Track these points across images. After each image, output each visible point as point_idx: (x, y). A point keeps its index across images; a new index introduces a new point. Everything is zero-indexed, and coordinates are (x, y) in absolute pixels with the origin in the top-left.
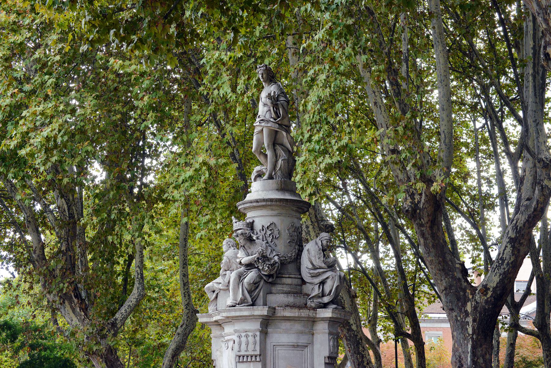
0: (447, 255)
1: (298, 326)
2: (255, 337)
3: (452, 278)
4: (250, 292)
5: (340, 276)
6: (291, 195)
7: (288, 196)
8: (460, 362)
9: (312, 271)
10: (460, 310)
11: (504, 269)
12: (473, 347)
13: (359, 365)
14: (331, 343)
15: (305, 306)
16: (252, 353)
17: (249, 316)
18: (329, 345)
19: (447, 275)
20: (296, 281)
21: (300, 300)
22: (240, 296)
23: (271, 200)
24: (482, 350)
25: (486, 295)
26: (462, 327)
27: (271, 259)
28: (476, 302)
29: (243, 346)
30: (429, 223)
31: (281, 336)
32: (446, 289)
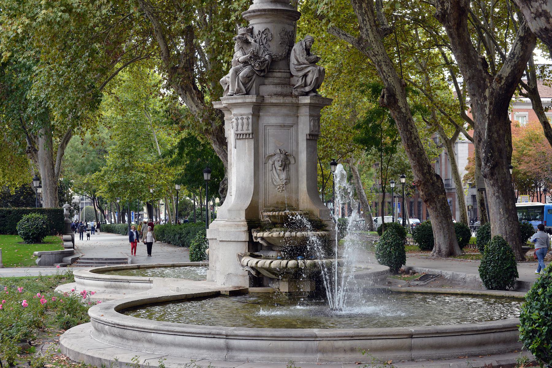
0: (471, 51)
1: (284, 111)
2: (248, 119)
3: (475, 69)
4: (244, 84)
5: (319, 70)
6: (282, 5)
7: (279, 7)
8: (479, 136)
9: (297, 67)
10: (481, 96)
11: (515, 62)
12: (489, 125)
13: (408, 140)
14: (312, 123)
15: (291, 95)
16: (246, 132)
17: (243, 103)
18: (310, 125)
19: (470, 67)
20: (284, 75)
21: (286, 90)
22: (236, 87)
23: (264, 10)
24: (496, 127)
25: (500, 83)
26: (482, 109)
27: (261, 57)
28: (493, 89)
29: (240, 126)
30: (456, 26)
31: (271, 119)
32: (469, 78)
